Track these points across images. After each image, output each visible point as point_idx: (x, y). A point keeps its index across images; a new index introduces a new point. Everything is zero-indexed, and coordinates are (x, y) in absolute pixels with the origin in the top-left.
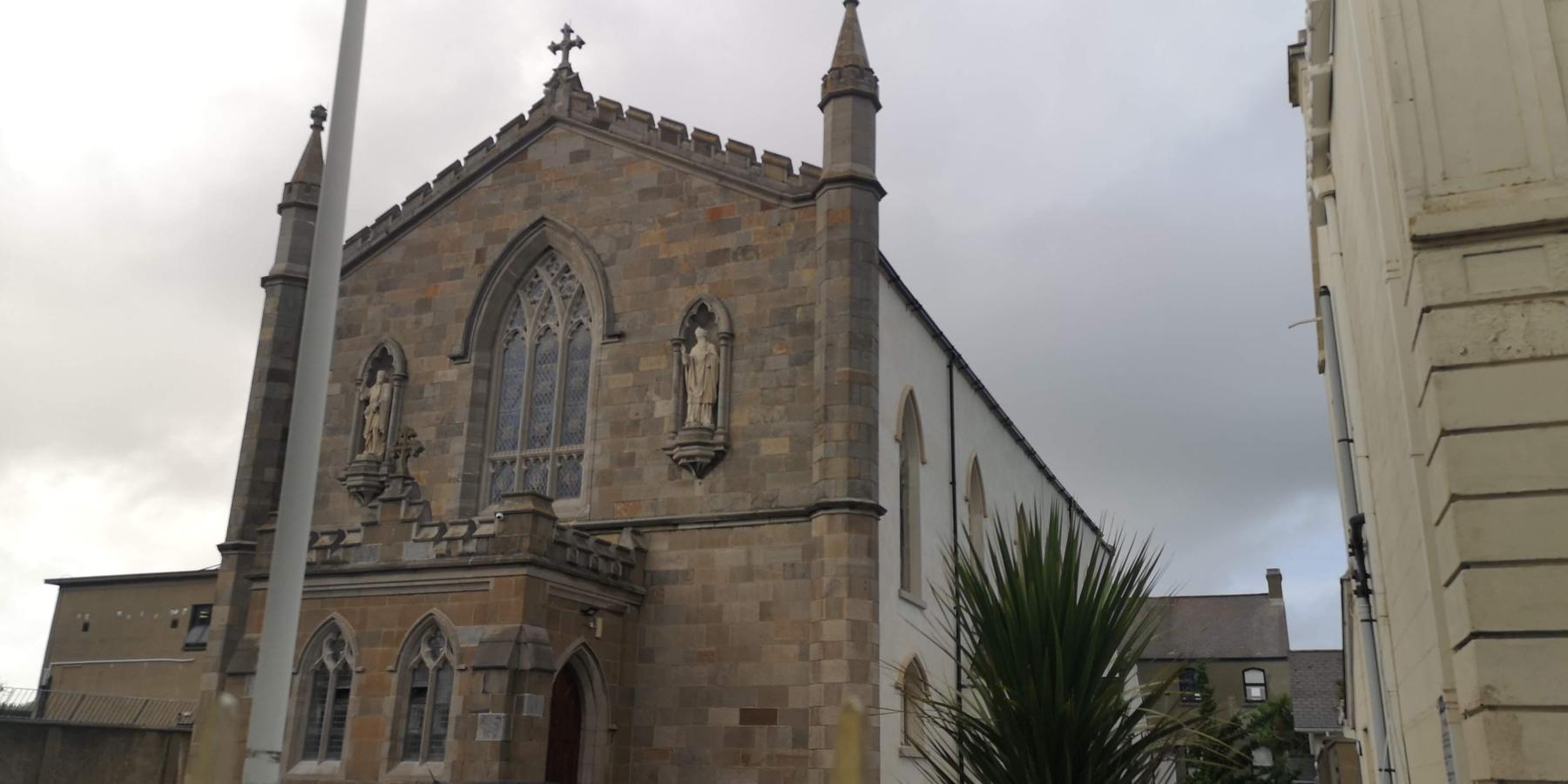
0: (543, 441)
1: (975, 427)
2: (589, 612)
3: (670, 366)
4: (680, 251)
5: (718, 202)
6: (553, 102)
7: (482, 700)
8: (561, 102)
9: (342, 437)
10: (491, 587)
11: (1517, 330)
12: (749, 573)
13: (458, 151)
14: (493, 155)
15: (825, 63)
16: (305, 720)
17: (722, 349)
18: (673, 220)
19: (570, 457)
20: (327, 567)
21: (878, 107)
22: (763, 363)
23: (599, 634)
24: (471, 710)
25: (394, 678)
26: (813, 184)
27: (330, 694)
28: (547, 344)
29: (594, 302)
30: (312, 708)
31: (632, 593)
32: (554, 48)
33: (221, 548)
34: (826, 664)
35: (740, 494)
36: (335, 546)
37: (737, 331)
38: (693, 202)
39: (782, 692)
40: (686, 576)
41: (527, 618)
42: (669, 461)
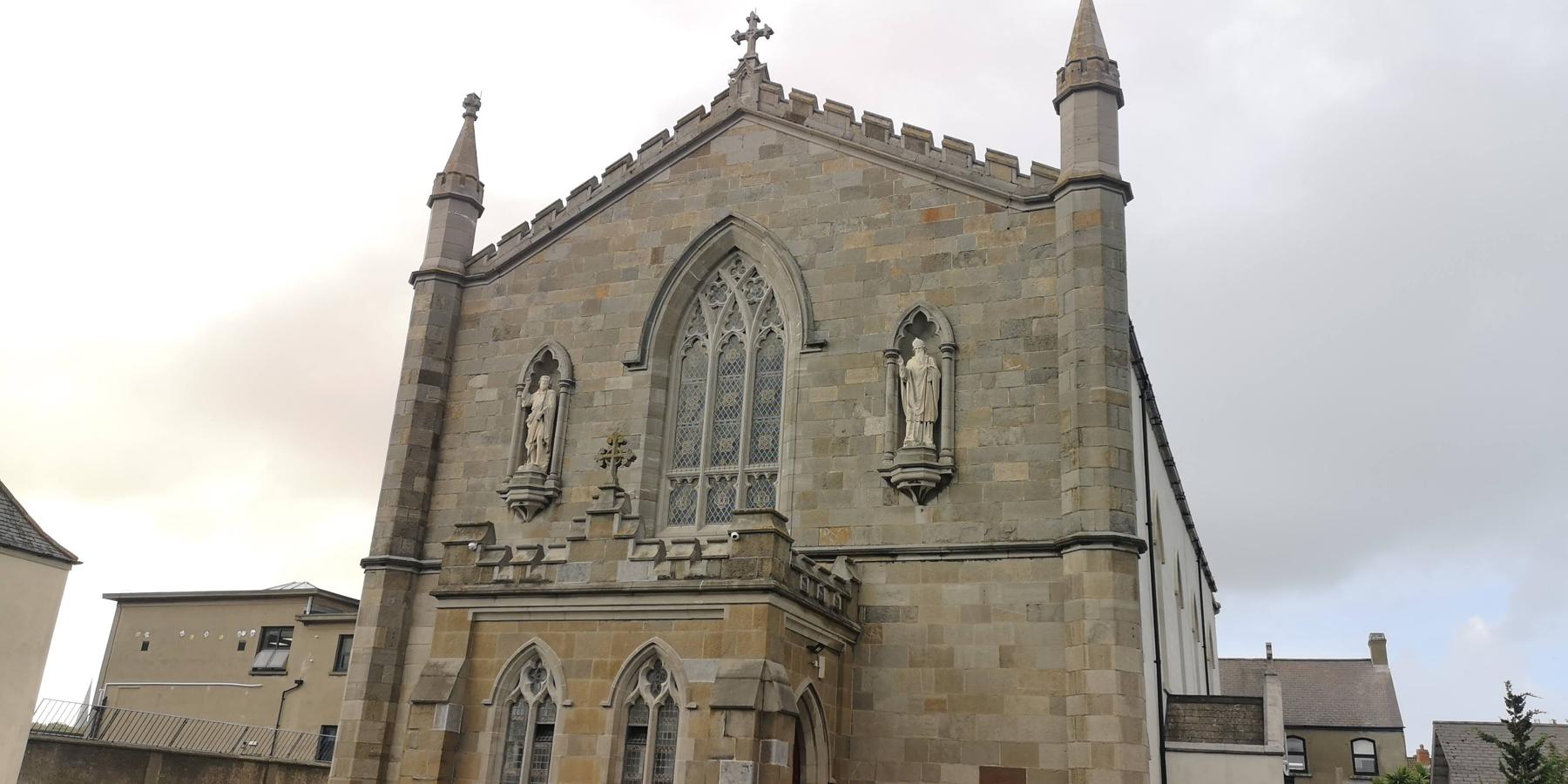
0: (730, 458)
2: (813, 649)
4: (890, 254)
6: (739, 93)
7: (724, 745)
9: (499, 446)
10: (726, 615)
12: (985, 613)
14: (672, 149)
17: (945, 363)
18: (883, 221)
19: (762, 477)
20: (527, 586)
22: (994, 379)
23: (822, 674)
26: (1044, 192)
28: (730, 355)
31: (850, 630)
32: (739, 38)
34: (1091, 719)
35: (970, 524)
37: (962, 344)
38: (904, 202)
39: (1031, 750)
40: (908, 614)
42: (885, 484)
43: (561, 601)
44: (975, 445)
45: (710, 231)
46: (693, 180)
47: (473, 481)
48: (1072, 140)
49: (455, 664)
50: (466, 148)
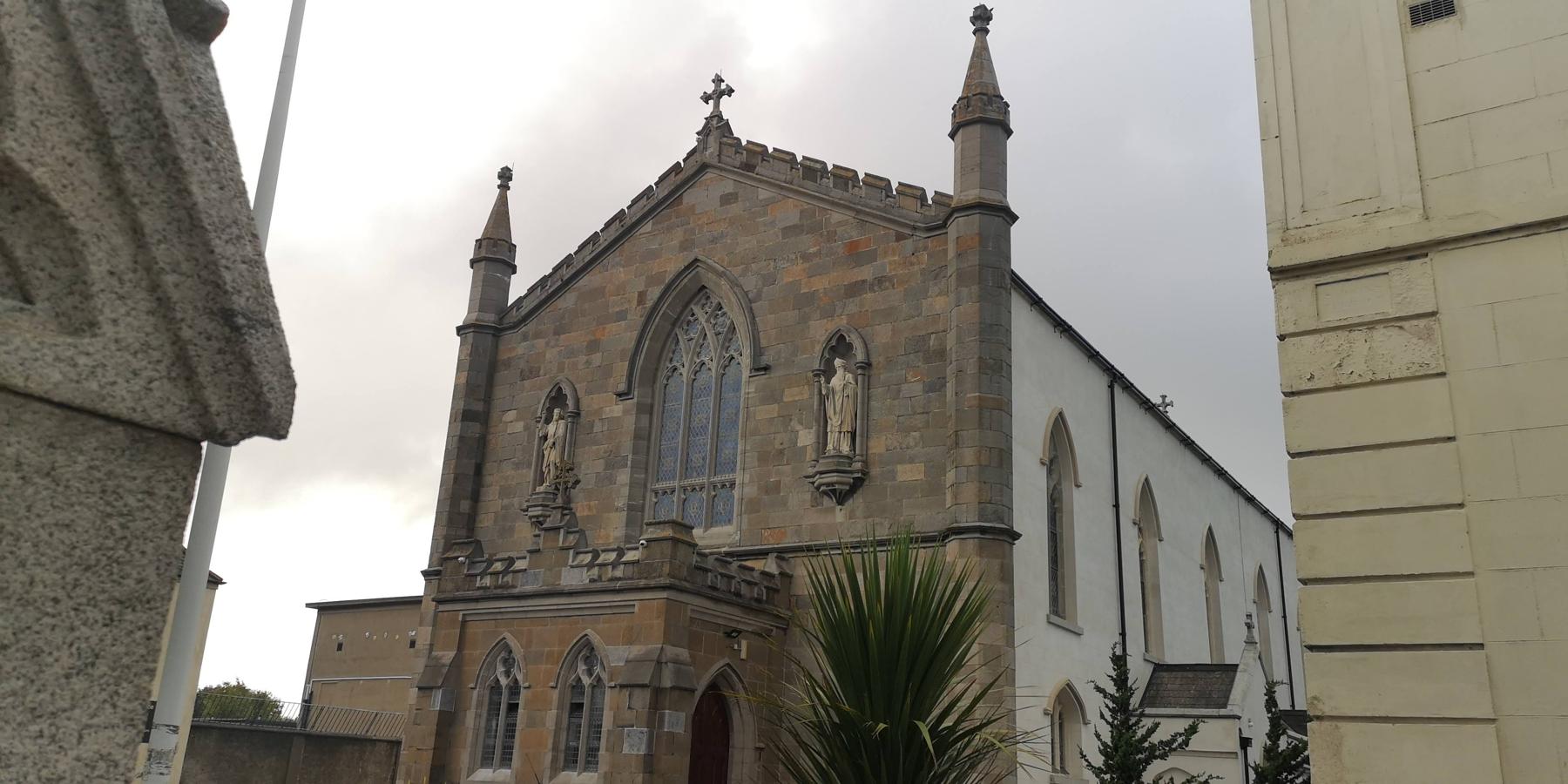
1: (1145, 453)
2: (732, 634)
3: (811, 397)
4: (820, 284)
5: (855, 235)
6: (705, 149)
7: (629, 716)
8: (712, 148)
10: (636, 609)
11: (1361, 354)
13: (621, 199)
15: (957, 91)
16: (482, 732)
18: (815, 255)
20: (499, 591)
21: (1009, 133)
22: (899, 391)
23: (743, 655)
24: (620, 725)
25: (555, 694)
26: (947, 209)
27: (503, 707)
29: (743, 340)
30: (489, 720)
32: (706, 98)
33: (425, 573)
35: (877, 520)
36: (505, 572)
41: (668, 638)
43: (523, 603)
44: (883, 450)
45: (680, 274)
46: (669, 229)
47: (506, 501)
48: (963, 168)
49: (448, 656)
50: (501, 214)
